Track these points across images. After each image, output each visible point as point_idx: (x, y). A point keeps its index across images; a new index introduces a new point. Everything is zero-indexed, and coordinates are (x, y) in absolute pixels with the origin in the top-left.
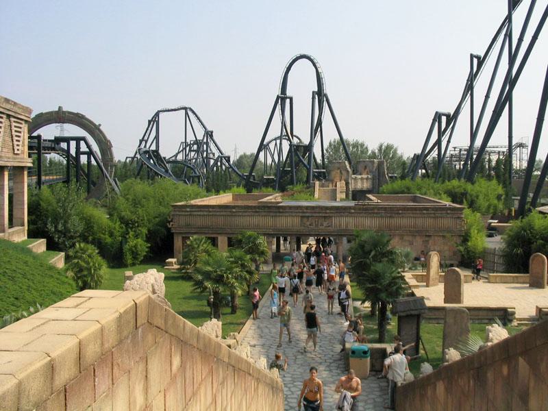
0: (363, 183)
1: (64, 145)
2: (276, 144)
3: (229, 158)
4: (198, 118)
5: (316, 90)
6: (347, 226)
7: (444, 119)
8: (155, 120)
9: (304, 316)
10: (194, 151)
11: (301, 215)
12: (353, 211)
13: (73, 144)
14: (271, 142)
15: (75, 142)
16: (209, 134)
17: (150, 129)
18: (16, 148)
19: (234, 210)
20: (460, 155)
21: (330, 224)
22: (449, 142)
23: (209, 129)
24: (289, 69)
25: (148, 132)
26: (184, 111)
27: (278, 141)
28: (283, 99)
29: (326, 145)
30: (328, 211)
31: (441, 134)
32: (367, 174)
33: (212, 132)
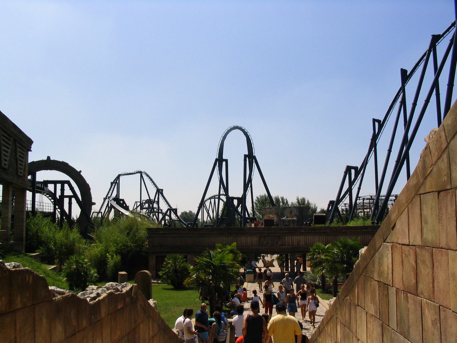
1: (51, 187)
2: (211, 202)
3: (176, 210)
4: (151, 180)
5: (247, 153)
7: (353, 171)
8: (116, 182)
9: (394, 230)
10: (145, 208)
13: (59, 186)
15: (60, 185)
16: (159, 192)
17: (112, 189)
18: (19, 170)
20: (363, 204)
22: (359, 188)
23: (160, 188)
24: (224, 138)
25: (111, 191)
26: (139, 174)
27: (213, 200)
28: (220, 161)
29: (255, 199)
30: (282, 232)
31: (351, 183)
33: (162, 190)
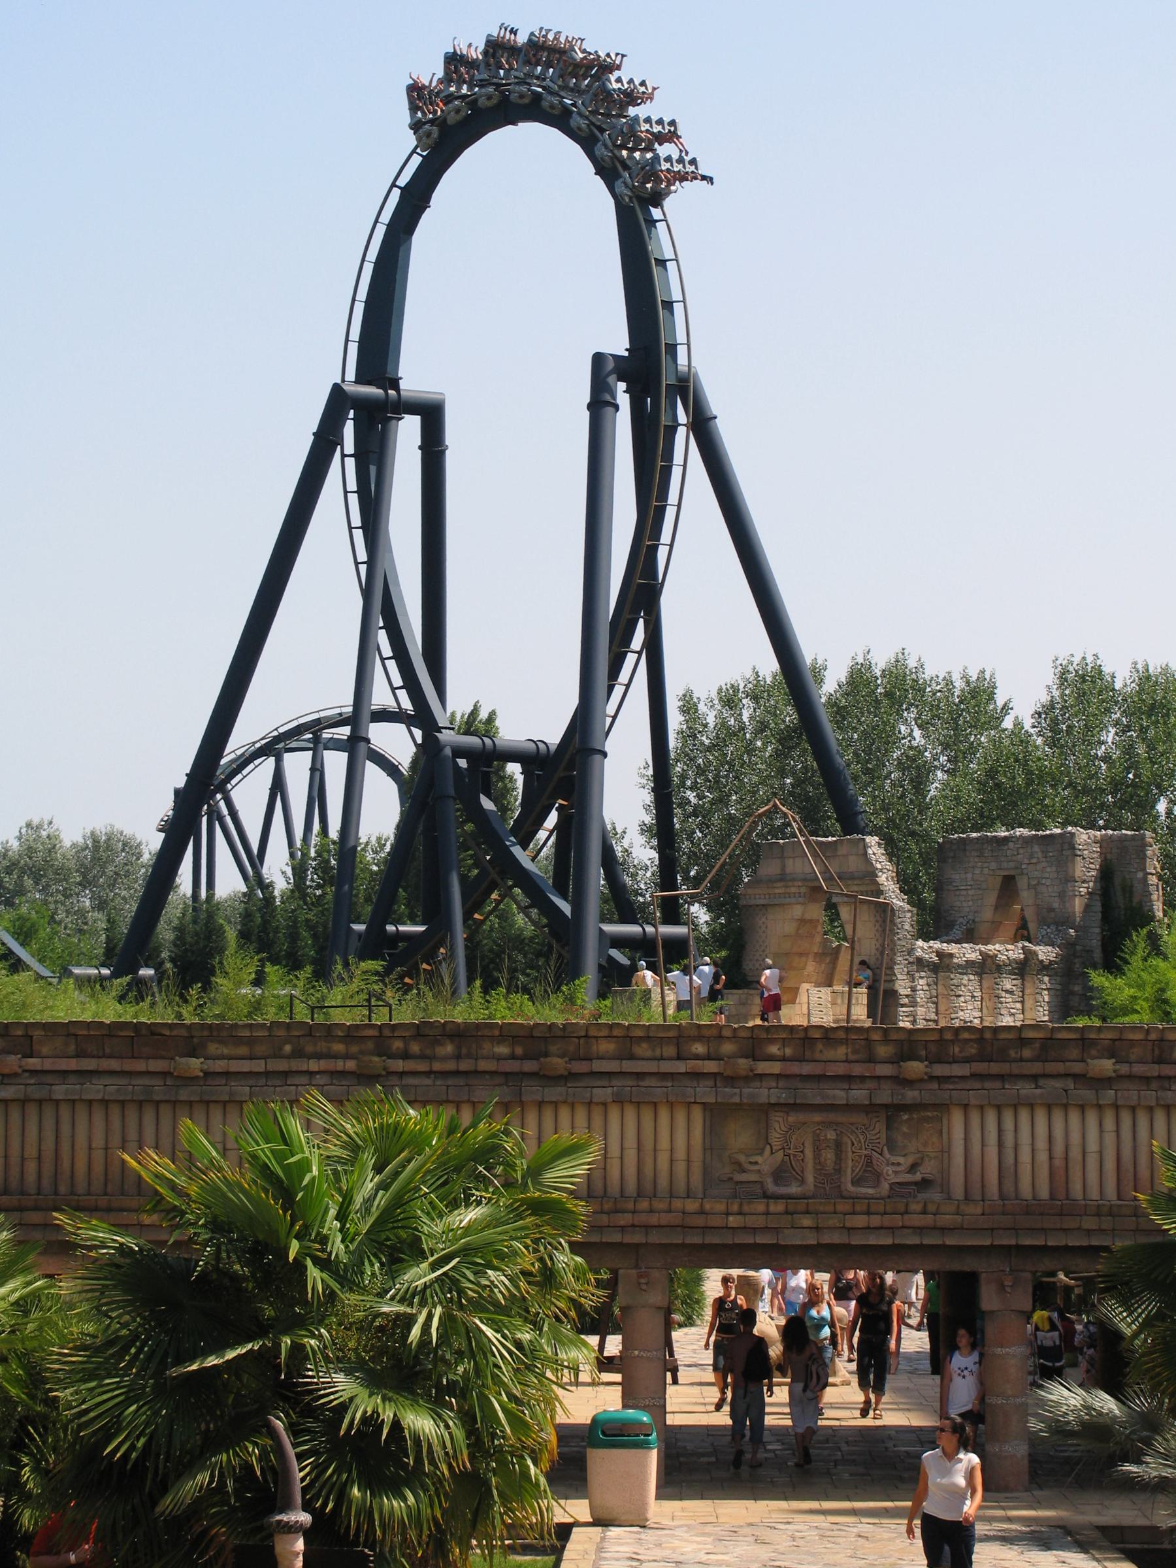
0: (993, 999)
2: (278, 786)
5: (618, 343)
6: (1060, 1174)
11: (705, 1092)
12: (1106, 1066)
14: (244, 762)
19: (195, 1064)
21: (928, 1169)
27: (297, 765)
32: (1022, 933)
